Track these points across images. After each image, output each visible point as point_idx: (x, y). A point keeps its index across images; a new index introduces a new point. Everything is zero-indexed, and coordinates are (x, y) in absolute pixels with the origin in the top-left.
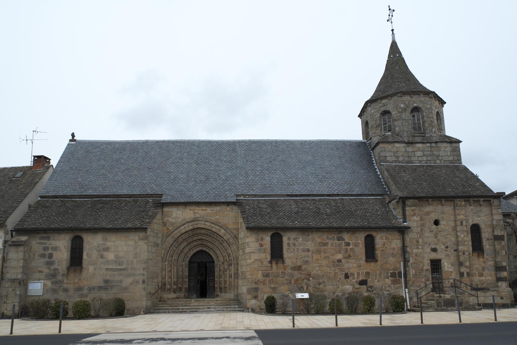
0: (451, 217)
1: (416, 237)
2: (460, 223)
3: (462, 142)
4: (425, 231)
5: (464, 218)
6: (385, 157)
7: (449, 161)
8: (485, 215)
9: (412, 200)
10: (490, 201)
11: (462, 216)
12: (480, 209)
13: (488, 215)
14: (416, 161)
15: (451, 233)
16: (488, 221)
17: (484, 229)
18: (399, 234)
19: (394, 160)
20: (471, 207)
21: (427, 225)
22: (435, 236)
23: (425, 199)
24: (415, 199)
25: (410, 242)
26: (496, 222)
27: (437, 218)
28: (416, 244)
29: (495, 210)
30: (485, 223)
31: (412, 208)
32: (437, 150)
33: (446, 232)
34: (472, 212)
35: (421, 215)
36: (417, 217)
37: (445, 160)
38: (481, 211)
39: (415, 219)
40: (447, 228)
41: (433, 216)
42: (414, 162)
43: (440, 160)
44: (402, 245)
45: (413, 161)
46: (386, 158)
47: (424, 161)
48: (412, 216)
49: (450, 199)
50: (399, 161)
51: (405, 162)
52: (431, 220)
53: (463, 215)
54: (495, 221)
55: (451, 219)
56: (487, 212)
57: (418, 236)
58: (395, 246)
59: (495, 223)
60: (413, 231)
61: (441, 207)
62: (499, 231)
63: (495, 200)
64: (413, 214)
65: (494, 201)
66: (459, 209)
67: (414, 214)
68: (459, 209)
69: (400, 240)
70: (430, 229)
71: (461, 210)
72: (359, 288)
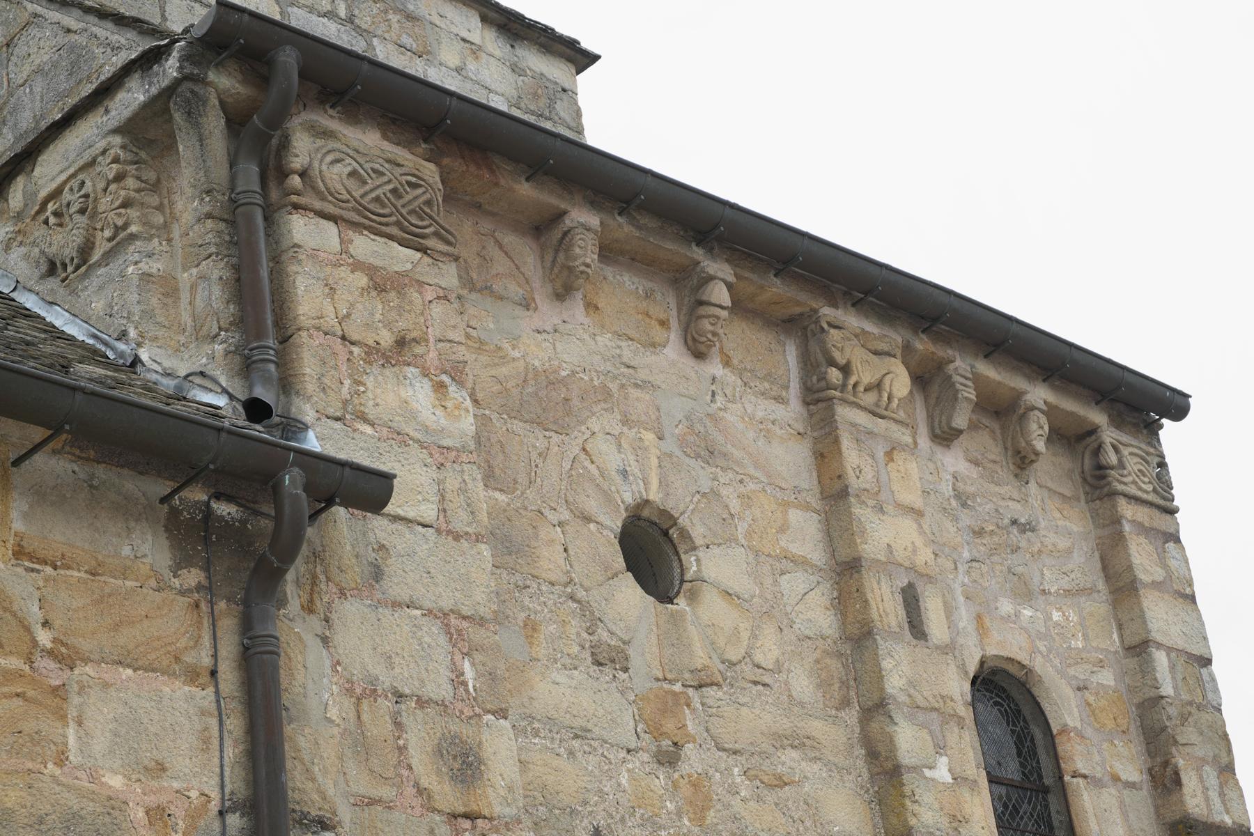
1: (439, 687)
3: (596, 58)
15: (817, 727)
18: (193, 577)
20: (953, 461)
22: (656, 732)
25: (360, 744)
28: (448, 796)
31: (365, 246)
32: (406, 40)
34: (966, 519)
36: (440, 387)
39: (413, 416)
44: (236, 783)
52: (592, 505)
57: (458, 680)
58: (116, 782)
60: (395, 588)
64: (386, 339)
67: (401, 343)
69: (206, 697)
70: (593, 622)
72: (116, 627)
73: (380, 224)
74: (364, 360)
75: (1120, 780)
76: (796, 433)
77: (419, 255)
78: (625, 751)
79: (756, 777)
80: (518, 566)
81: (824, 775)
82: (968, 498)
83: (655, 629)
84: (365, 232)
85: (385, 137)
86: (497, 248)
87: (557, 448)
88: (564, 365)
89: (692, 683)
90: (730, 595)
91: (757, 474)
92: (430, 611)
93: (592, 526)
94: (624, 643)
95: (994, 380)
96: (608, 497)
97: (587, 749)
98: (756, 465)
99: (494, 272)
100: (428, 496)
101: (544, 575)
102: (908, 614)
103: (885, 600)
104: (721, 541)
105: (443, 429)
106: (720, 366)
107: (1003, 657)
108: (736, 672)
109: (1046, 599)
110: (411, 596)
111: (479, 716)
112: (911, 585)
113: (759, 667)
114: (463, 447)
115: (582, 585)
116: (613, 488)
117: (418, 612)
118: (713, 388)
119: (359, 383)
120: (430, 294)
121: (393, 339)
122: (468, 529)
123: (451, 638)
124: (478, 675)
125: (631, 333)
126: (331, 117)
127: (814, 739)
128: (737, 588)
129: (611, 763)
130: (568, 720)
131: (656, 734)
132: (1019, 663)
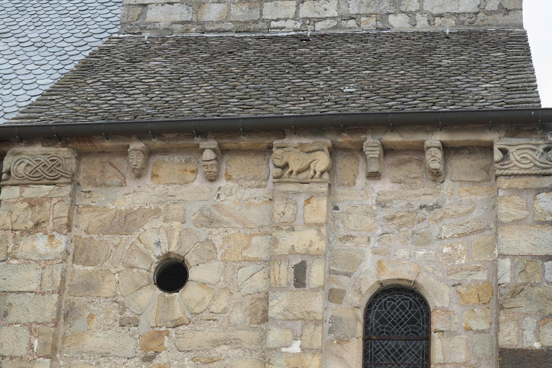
0: (255, 240)
2: (291, 277)
4: (91, 317)
5: (322, 245)
6: (139, 10)
7: (456, 15)
8: (461, 230)
9: (38, 149)
10: (488, 148)
11: (311, 235)
12: (430, 201)
13: (481, 231)
14: (286, 20)
15: (241, 334)
16: (478, 269)
17: (446, 311)
19: (178, 18)
21: (108, 289)
23: (107, 144)
24: (53, 145)
26: (513, 268)
27: (174, 249)
29: (517, 199)
30: (458, 278)
31: (30, 192)
33: (215, 325)
34: (383, 213)
35: (87, 232)
36: (52, 237)
37: (435, 12)
38: (437, 206)
40: (222, 303)
41: (151, 237)
42: (274, 24)
43: (408, 13)
45: (269, 21)
46: (142, 15)
47: (328, 22)
48: (28, 232)
49: (245, 142)
50: (202, 24)
51: (230, 26)
52: (137, 261)
53: (318, 226)
54: (507, 263)
55: (251, 255)
56: (475, 214)
57: (31, 347)
59: (506, 279)
61: (206, 186)
62: (530, 323)
63: (514, 141)
64: (30, 224)
65: (511, 150)
66: (296, 193)
67: (37, 225)
68: (296, 193)
70: (123, 308)
71: (308, 201)
73: (37, 180)
74: (20, 236)
75: (471, 330)
76: (268, 200)
77: (54, 186)
78: (126, 359)
79: (198, 360)
80: (91, 294)
81: (240, 355)
82: (386, 202)
83: (156, 307)
84: (30, 186)
85: (43, 146)
86: (110, 166)
87: (125, 241)
88: (136, 205)
89: (172, 326)
90: (205, 284)
91: (237, 226)
92: (24, 324)
93: (135, 270)
94: (138, 315)
95: (398, 142)
96: (146, 256)
97: (106, 360)
98: (237, 221)
99: (107, 176)
100: (34, 281)
101: (103, 296)
102: (296, 276)
103: (281, 272)
104: (205, 261)
105: (48, 253)
106: (225, 181)
107: (394, 279)
108: (198, 317)
109: (441, 242)
110: (17, 320)
111: (35, 359)
112: (303, 263)
113: (213, 313)
114: (56, 258)
115: (122, 296)
116: (150, 251)
117: (19, 325)
118: (219, 192)
119: (17, 244)
120: (55, 201)
121: (34, 224)
122: (49, 290)
123: (31, 333)
124: (39, 344)
125: (173, 181)
126: (22, 146)
127: (238, 339)
128: (209, 281)
129: (117, 364)
130: (101, 350)
131: (145, 350)
132: (407, 280)
